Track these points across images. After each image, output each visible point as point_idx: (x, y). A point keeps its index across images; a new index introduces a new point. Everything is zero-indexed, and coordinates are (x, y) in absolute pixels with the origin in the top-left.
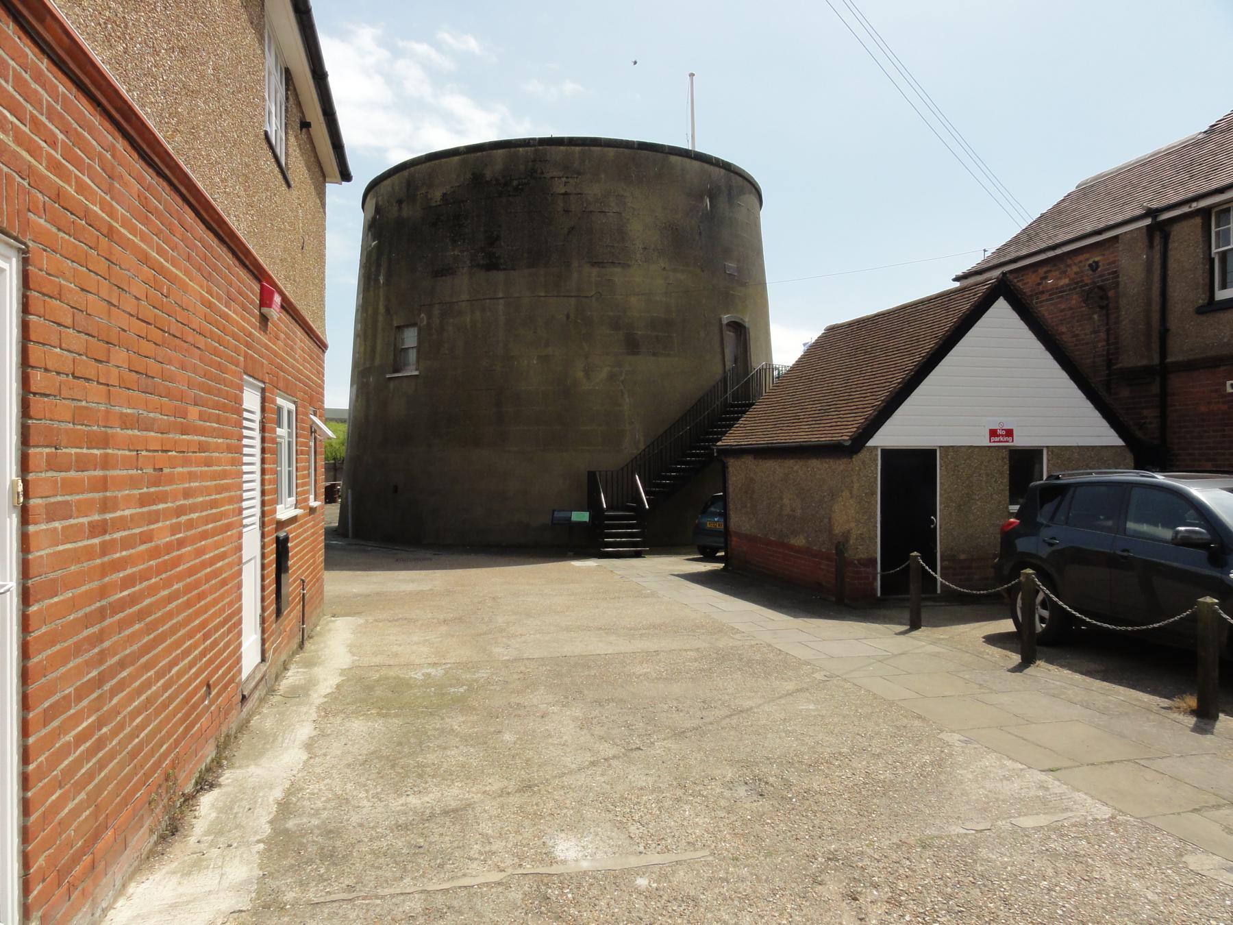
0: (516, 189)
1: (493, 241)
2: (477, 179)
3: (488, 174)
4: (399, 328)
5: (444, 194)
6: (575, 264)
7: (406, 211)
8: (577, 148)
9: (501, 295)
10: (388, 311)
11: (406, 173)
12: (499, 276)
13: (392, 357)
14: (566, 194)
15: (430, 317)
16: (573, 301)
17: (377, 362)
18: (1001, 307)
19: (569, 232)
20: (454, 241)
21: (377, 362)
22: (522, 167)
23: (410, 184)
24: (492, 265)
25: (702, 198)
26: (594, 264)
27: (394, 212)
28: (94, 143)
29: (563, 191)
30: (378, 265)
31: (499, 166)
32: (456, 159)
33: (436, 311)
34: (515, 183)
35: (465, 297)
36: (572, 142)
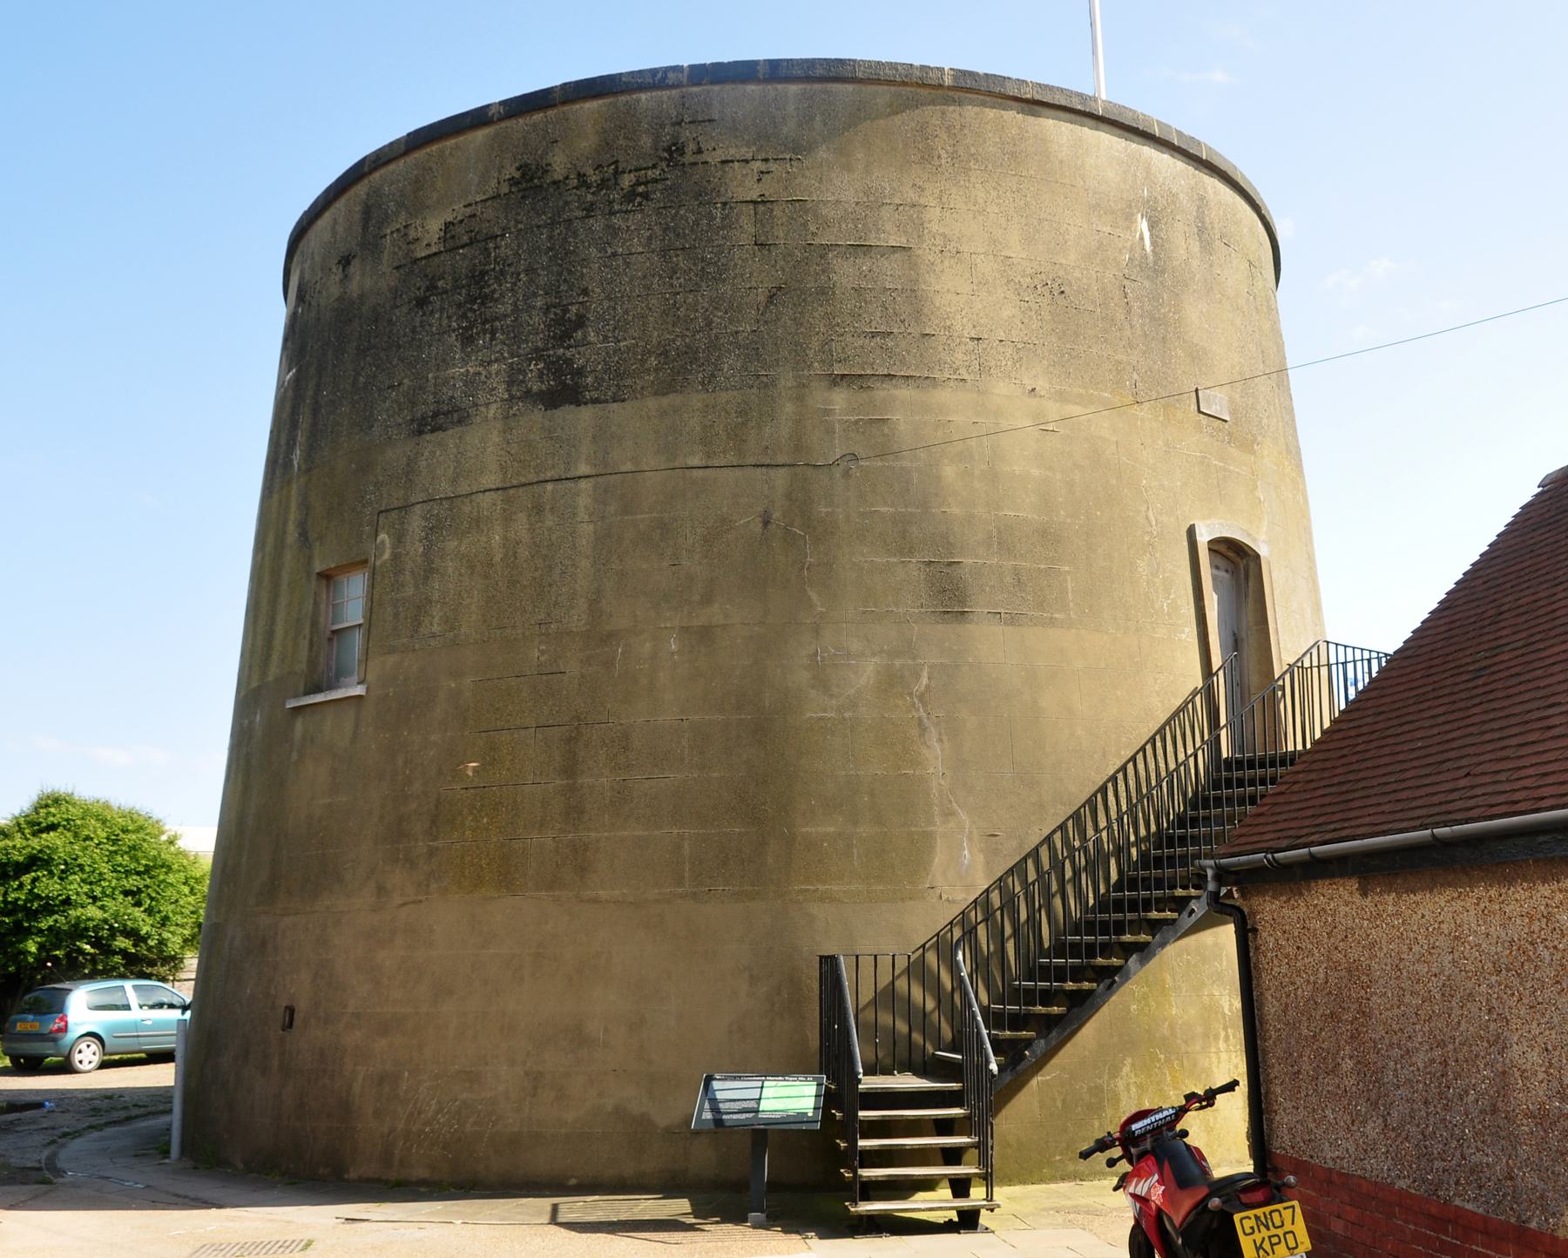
0: (631, 196)
1: (566, 328)
2: (530, 182)
3: (559, 163)
4: (327, 577)
5: (448, 225)
6: (786, 380)
7: (361, 280)
8: (793, 88)
9: (583, 469)
10: (304, 535)
11: (361, 189)
12: (585, 416)
13: (304, 653)
14: (763, 201)
15: (399, 539)
16: (780, 477)
17: (273, 671)
18: (561, 1219)
19: (771, 298)
20: (467, 340)
21: (273, 671)
22: (646, 142)
23: (370, 214)
24: (564, 390)
25: (1129, 218)
26: (836, 381)
27: (333, 288)
28: (1242, 858)
29: (754, 196)
30: (294, 425)
31: (587, 143)
32: (481, 135)
33: (416, 523)
34: (627, 181)
35: (491, 480)
36: (777, 71)
